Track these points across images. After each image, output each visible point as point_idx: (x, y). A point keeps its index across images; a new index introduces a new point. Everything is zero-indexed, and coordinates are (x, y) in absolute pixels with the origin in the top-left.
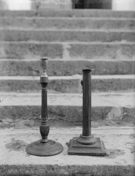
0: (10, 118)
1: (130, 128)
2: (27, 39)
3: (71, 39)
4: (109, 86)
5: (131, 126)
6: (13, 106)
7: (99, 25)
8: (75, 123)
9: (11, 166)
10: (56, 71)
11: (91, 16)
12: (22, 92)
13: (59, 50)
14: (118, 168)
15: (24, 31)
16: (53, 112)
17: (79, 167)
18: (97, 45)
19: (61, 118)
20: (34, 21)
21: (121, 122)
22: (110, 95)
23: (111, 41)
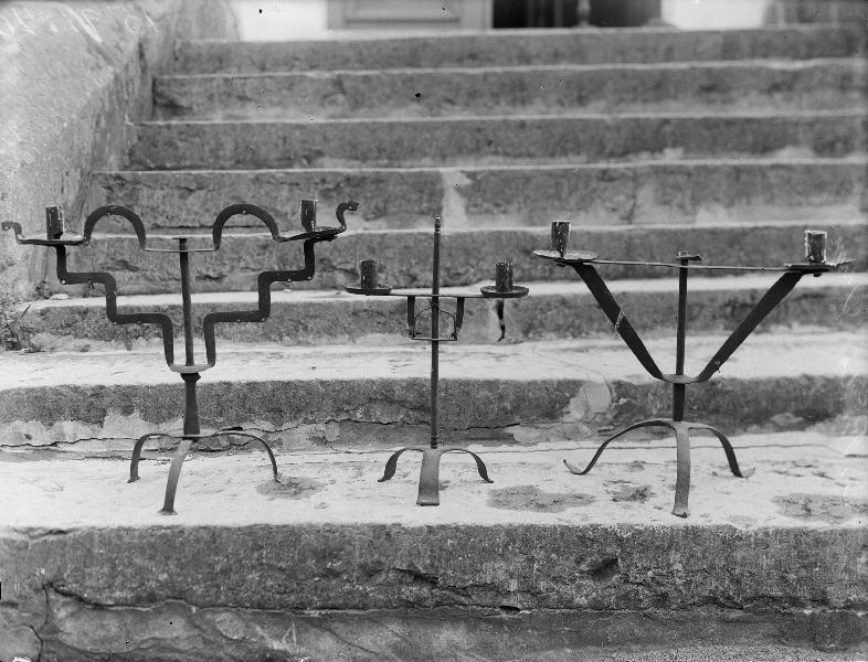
0: (266, 419)
1: (636, 445)
2: (311, 157)
3: (476, 151)
4: (591, 319)
5: (642, 440)
6: (273, 383)
7: (581, 91)
8: (467, 432)
9: (278, 527)
10: (415, 270)
11: (556, 57)
12: (299, 343)
13: (428, 194)
14: (562, 534)
15: (300, 127)
16: (396, 398)
17: (457, 528)
18: (565, 174)
19: (422, 419)
20: (338, 83)
21: (612, 428)
22: (594, 347)
23: (625, 153)
